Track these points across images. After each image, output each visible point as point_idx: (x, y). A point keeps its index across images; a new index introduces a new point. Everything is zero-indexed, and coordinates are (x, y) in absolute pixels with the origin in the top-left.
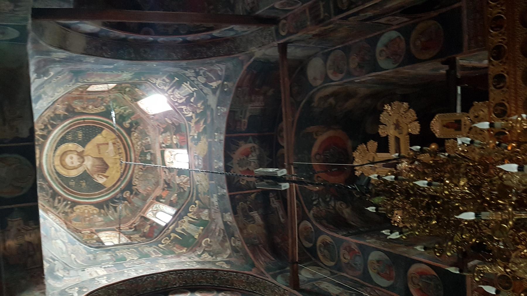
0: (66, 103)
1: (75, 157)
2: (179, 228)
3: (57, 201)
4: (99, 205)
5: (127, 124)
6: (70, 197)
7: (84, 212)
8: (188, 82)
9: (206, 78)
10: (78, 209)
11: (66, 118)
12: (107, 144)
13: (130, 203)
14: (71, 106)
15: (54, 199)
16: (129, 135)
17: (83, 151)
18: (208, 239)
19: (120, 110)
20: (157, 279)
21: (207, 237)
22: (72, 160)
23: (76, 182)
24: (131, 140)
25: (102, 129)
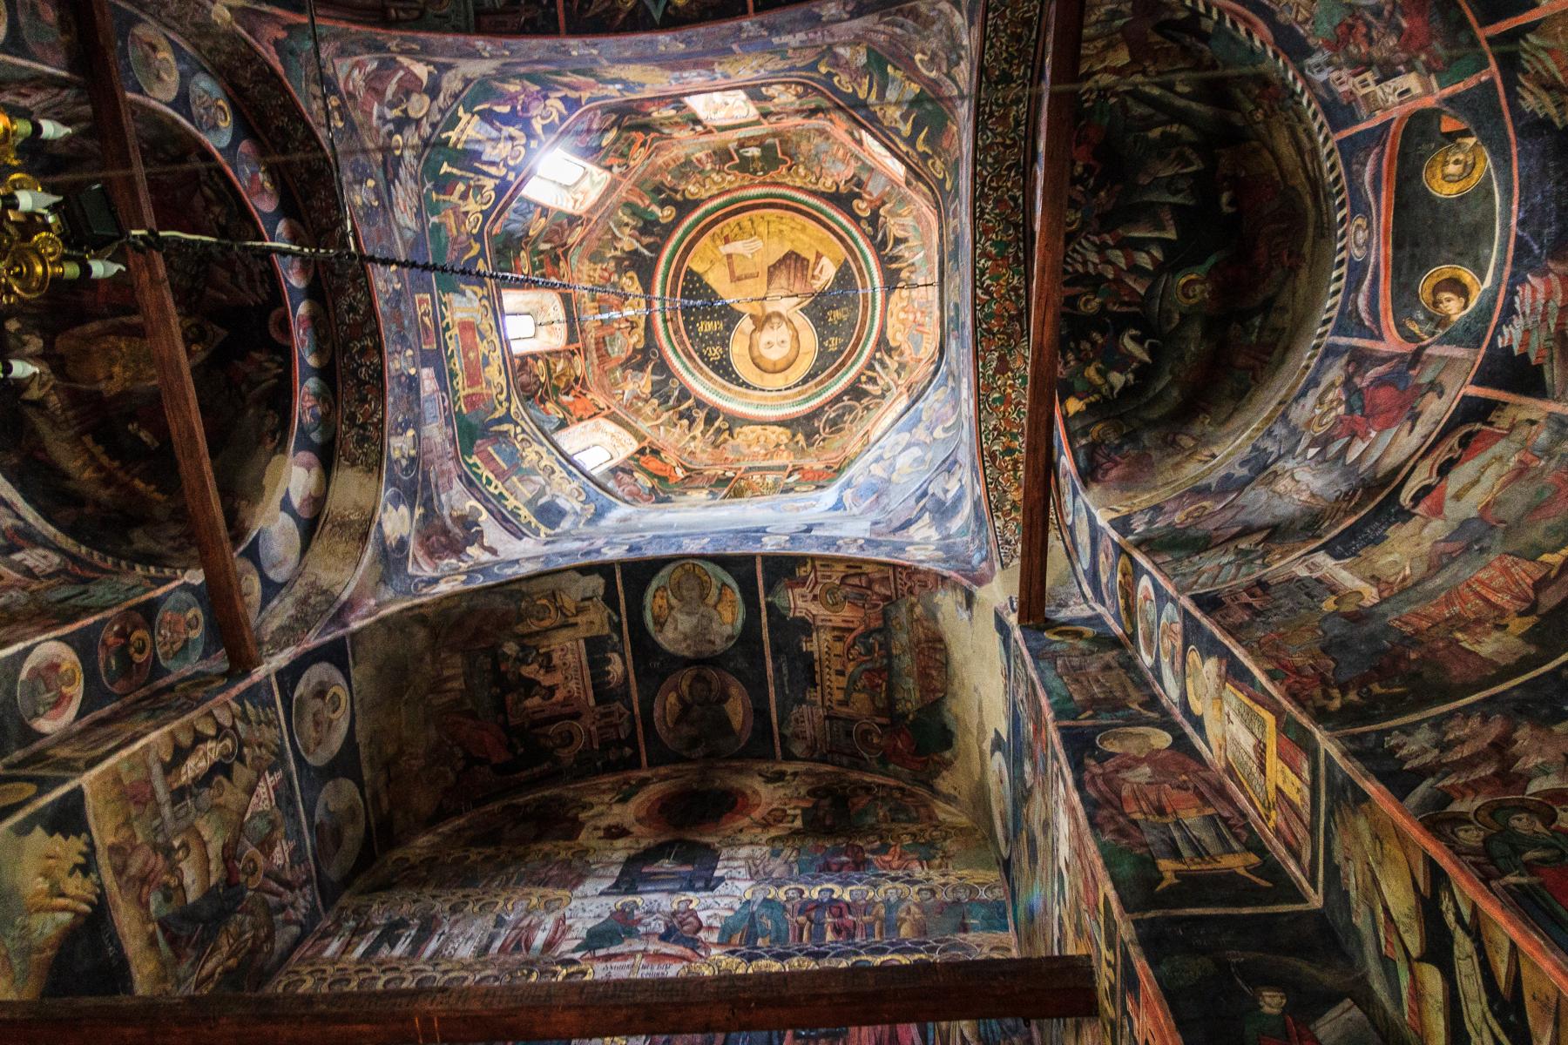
0: (618, 374)
1: (766, 336)
2: (901, 126)
3: (869, 387)
4: (892, 281)
5: (666, 214)
6: (867, 352)
7: (903, 322)
8: (444, 136)
9: (408, 94)
10: (896, 336)
11: (663, 367)
12: (729, 256)
13: (884, 203)
14: (629, 359)
15: (866, 393)
16: (696, 204)
17: (752, 316)
18: (918, 57)
19: (626, 239)
20: (988, 256)
21: (913, 59)
22: (774, 346)
23: (832, 334)
24: (711, 198)
25: (690, 272)
